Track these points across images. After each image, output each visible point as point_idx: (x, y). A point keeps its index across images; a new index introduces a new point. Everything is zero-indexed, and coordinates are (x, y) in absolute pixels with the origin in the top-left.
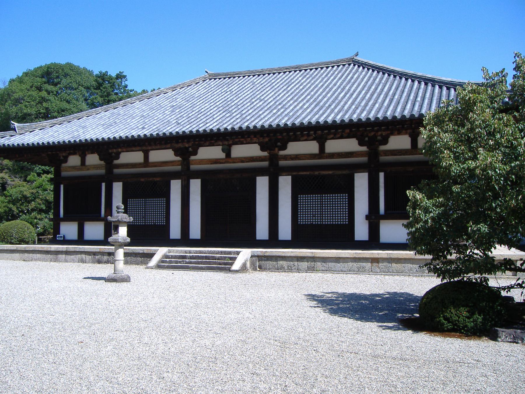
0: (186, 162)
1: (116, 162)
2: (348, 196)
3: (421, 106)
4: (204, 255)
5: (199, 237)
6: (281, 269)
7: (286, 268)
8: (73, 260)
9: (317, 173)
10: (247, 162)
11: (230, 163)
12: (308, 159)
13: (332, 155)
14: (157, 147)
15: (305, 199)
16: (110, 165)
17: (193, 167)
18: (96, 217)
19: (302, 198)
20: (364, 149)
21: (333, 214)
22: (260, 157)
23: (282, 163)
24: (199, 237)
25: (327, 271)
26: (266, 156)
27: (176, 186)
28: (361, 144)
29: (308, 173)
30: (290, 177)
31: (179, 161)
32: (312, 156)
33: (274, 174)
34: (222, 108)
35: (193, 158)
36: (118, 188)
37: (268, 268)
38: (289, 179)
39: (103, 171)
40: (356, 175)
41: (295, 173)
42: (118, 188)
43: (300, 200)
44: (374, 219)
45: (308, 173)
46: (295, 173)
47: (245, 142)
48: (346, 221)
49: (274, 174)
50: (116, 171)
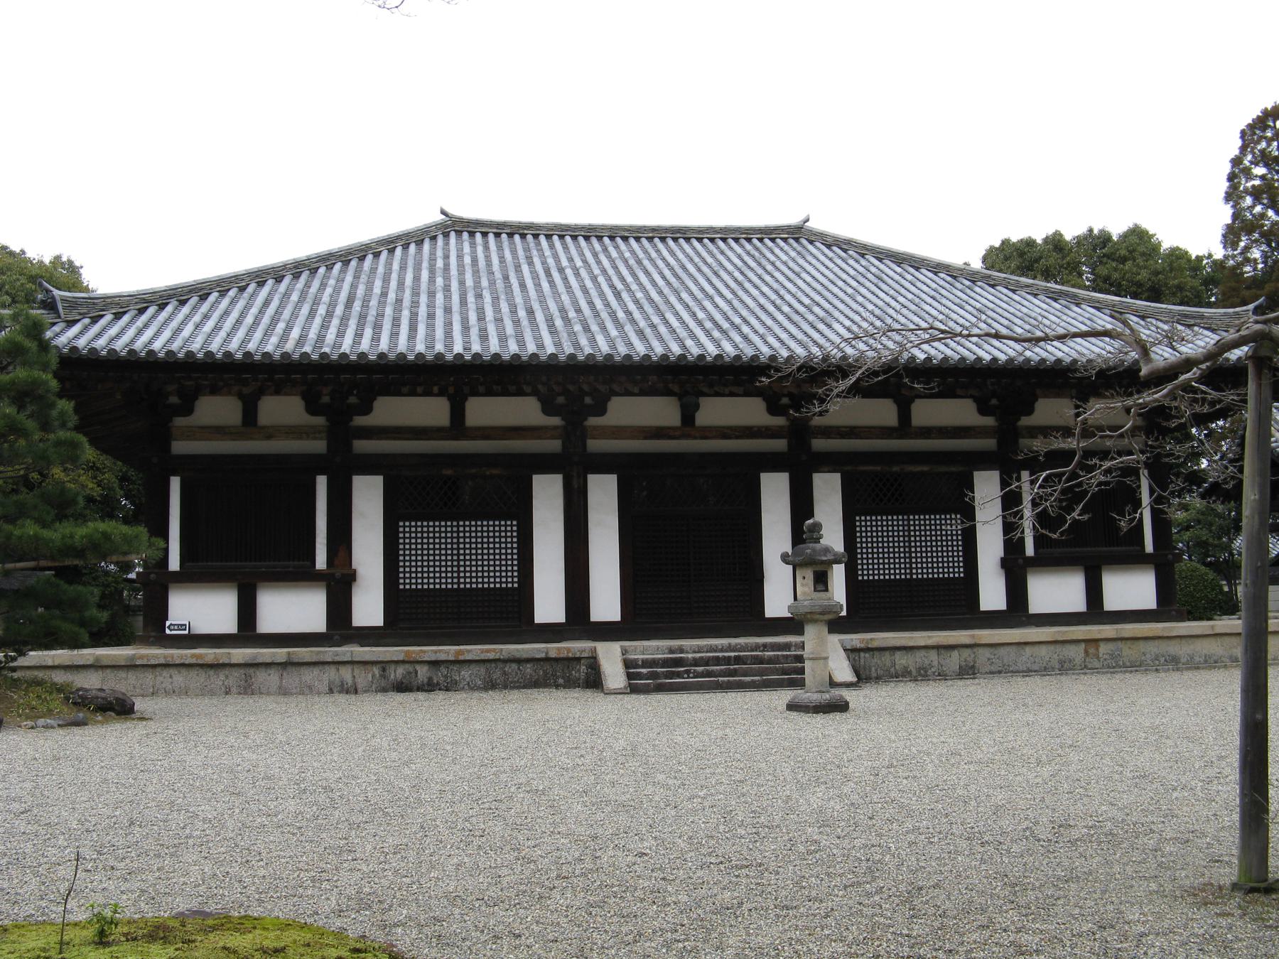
0: (574, 432)
1: (1025, 421)
2: (517, 526)
3: (394, 335)
4: (732, 654)
5: (616, 616)
6: (903, 676)
7: (914, 673)
8: (310, 688)
9: (896, 469)
10: (737, 437)
11: (695, 438)
12: (877, 438)
13: (927, 432)
14: (727, 391)
15: (470, 532)
16: (341, 430)
17: (595, 445)
18: (297, 572)
19: (405, 527)
20: (989, 421)
21: (471, 566)
22: (767, 428)
23: (819, 444)
24: (616, 616)
25: (1000, 672)
26: (781, 427)
27: (547, 497)
28: (983, 411)
29: (879, 468)
30: (839, 475)
31: (555, 428)
32: (885, 432)
33: (575, 470)
34: (901, 299)
35: (593, 421)
36: (368, 498)
37: (874, 675)
38: (836, 479)
39: (318, 446)
40: (976, 474)
41: (849, 468)
42: (368, 498)
43: (404, 532)
44: (1016, 570)
45: (879, 468)
46: (849, 468)
47: (481, 389)
48: (405, 584)
49: (575, 470)
50: (362, 446)
